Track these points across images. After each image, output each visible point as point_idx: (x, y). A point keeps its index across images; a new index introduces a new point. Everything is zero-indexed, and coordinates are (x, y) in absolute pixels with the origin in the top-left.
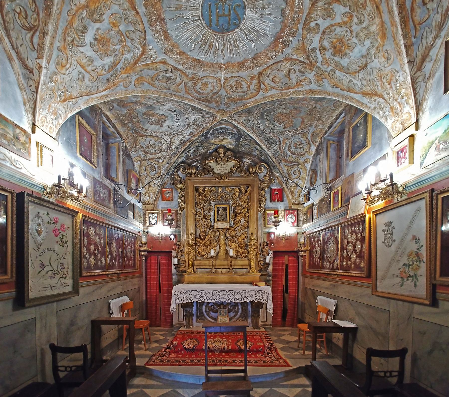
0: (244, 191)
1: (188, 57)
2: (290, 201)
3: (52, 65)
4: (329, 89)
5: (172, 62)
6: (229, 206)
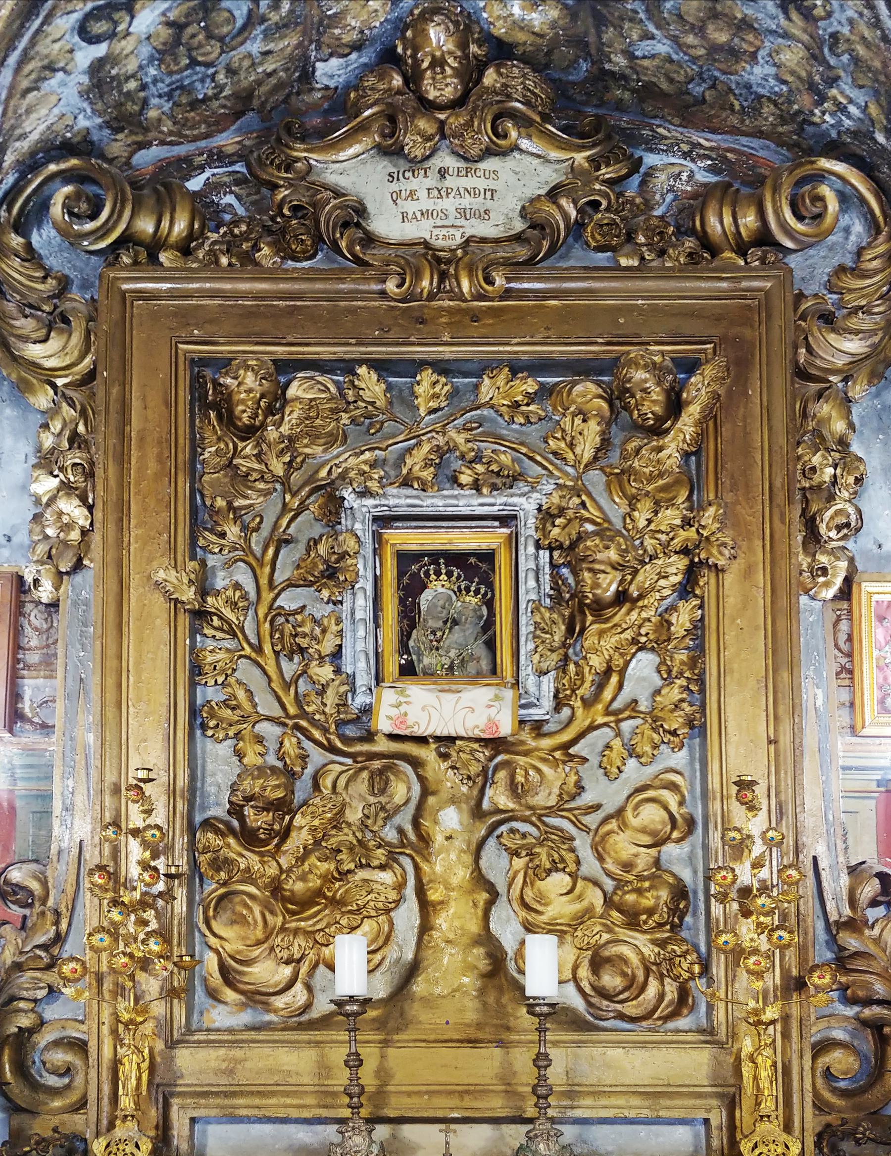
6: (513, 541)
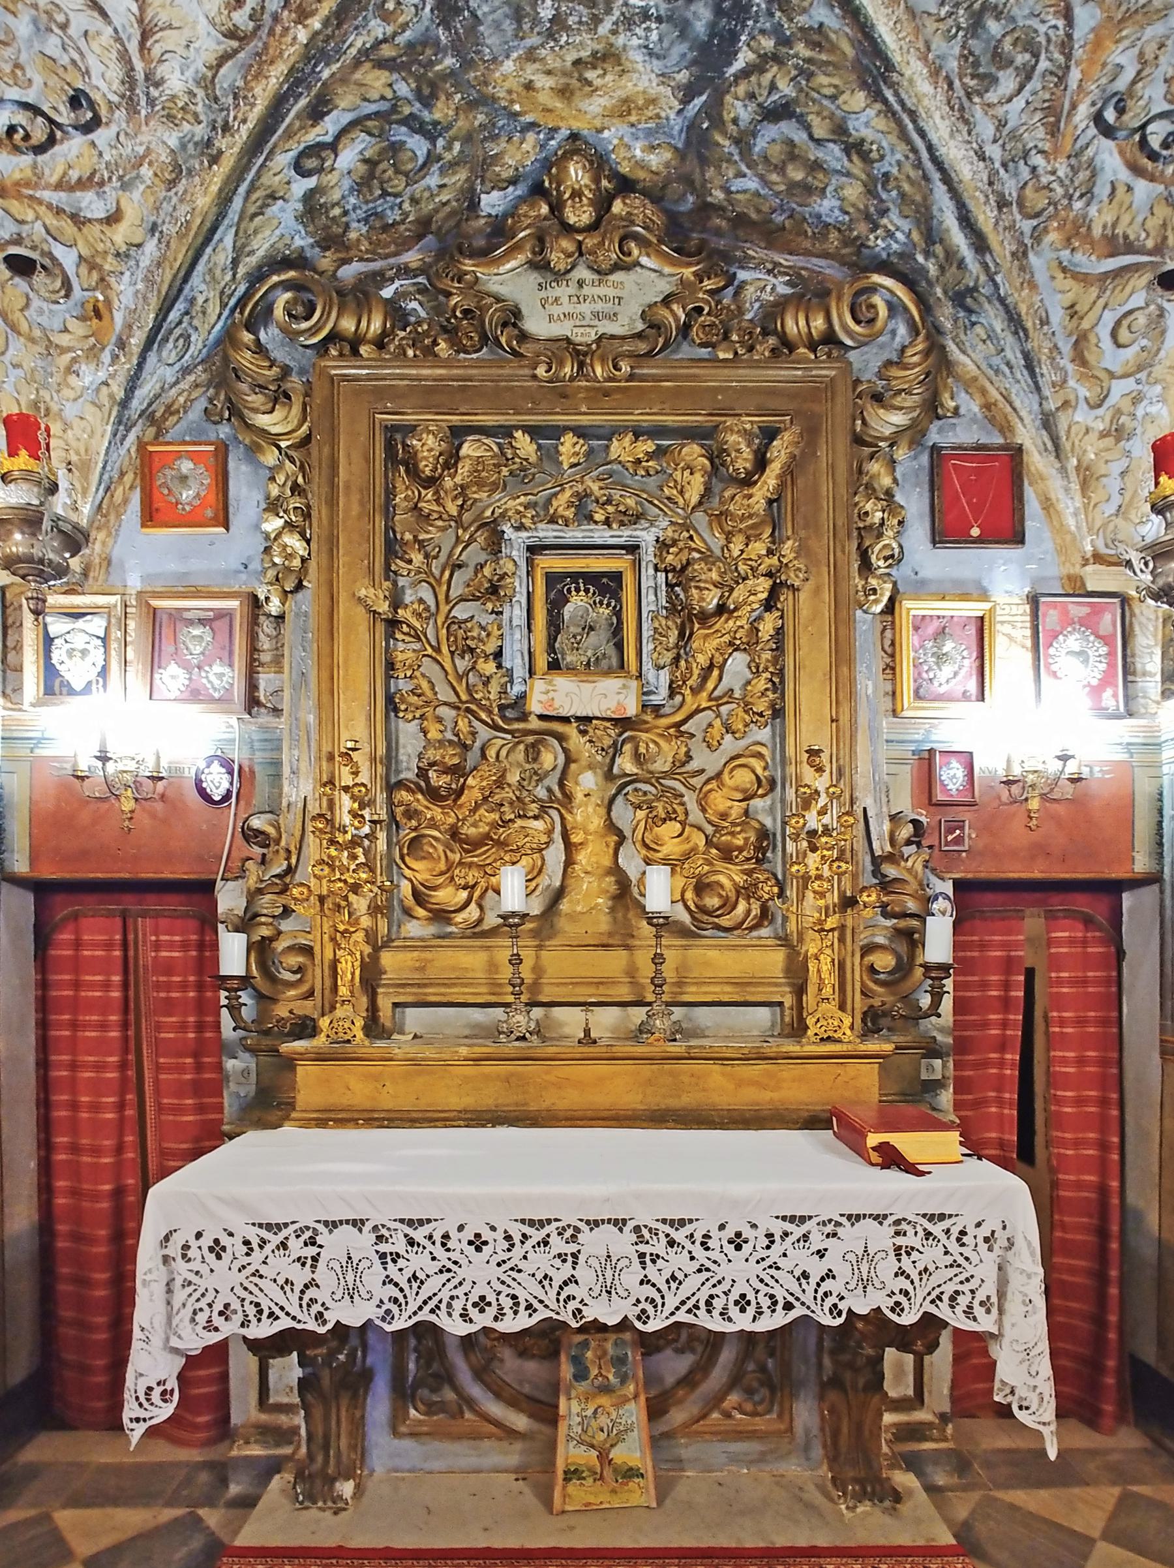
0: (743, 461)
2: (1064, 546)
6: (637, 565)
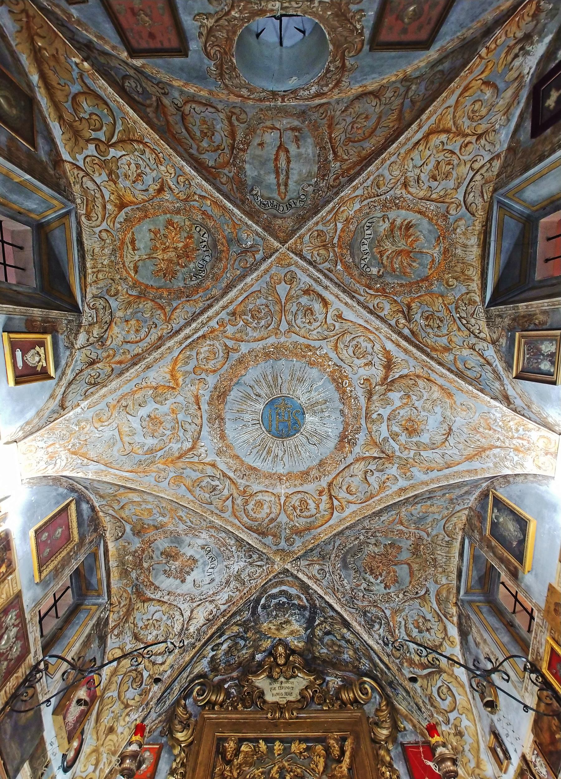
0: (336, 752)
1: (242, 463)
3: (91, 412)
4: (425, 478)
5: (222, 467)
